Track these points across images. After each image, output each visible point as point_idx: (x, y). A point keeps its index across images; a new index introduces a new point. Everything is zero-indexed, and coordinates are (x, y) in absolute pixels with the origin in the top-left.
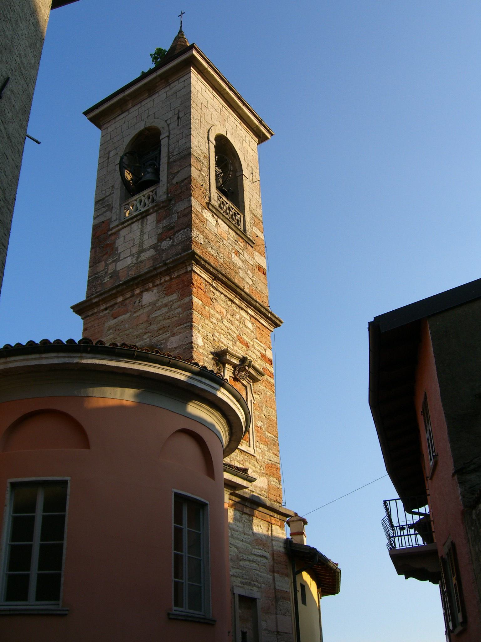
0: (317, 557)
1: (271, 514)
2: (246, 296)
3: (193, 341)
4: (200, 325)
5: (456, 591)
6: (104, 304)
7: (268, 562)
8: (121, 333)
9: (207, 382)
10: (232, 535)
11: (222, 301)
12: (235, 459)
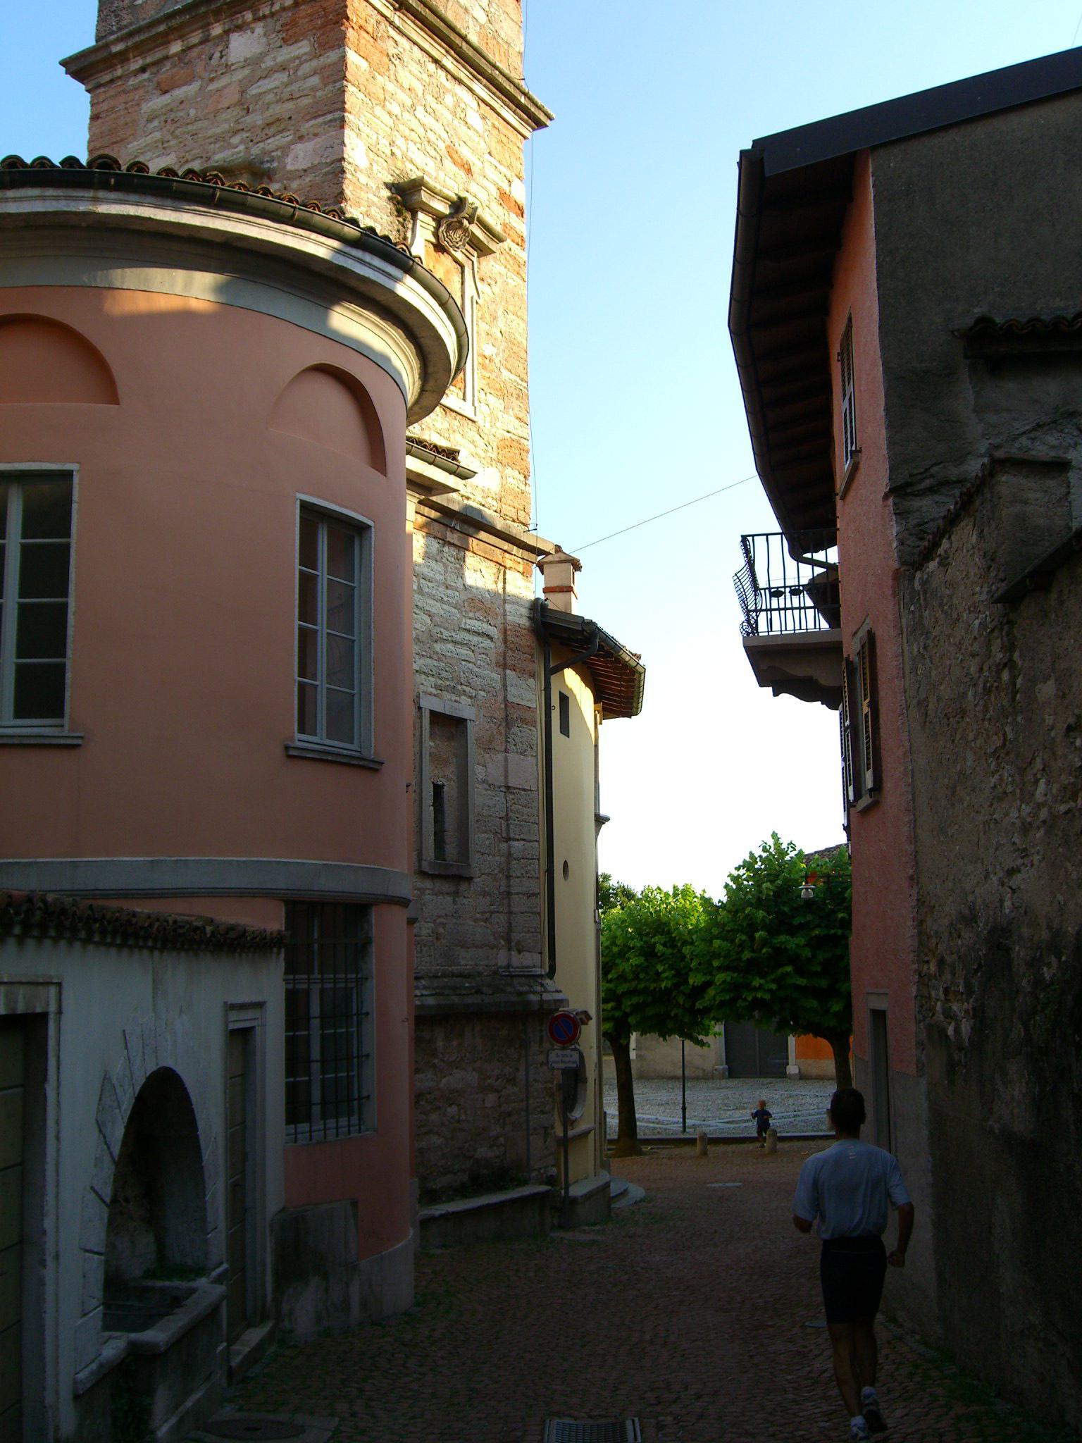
0: (597, 640)
1: (505, 548)
2: (470, 52)
3: (345, 156)
4: (363, 119)
5: (867, 727)
6: (139, 58)
7: (493, 647)
8: (180, 130)
9: (377, 262)
10: (420, 587)
11: (415, 61)
12: (433, 428)
